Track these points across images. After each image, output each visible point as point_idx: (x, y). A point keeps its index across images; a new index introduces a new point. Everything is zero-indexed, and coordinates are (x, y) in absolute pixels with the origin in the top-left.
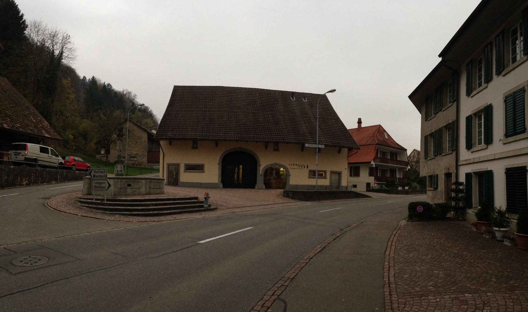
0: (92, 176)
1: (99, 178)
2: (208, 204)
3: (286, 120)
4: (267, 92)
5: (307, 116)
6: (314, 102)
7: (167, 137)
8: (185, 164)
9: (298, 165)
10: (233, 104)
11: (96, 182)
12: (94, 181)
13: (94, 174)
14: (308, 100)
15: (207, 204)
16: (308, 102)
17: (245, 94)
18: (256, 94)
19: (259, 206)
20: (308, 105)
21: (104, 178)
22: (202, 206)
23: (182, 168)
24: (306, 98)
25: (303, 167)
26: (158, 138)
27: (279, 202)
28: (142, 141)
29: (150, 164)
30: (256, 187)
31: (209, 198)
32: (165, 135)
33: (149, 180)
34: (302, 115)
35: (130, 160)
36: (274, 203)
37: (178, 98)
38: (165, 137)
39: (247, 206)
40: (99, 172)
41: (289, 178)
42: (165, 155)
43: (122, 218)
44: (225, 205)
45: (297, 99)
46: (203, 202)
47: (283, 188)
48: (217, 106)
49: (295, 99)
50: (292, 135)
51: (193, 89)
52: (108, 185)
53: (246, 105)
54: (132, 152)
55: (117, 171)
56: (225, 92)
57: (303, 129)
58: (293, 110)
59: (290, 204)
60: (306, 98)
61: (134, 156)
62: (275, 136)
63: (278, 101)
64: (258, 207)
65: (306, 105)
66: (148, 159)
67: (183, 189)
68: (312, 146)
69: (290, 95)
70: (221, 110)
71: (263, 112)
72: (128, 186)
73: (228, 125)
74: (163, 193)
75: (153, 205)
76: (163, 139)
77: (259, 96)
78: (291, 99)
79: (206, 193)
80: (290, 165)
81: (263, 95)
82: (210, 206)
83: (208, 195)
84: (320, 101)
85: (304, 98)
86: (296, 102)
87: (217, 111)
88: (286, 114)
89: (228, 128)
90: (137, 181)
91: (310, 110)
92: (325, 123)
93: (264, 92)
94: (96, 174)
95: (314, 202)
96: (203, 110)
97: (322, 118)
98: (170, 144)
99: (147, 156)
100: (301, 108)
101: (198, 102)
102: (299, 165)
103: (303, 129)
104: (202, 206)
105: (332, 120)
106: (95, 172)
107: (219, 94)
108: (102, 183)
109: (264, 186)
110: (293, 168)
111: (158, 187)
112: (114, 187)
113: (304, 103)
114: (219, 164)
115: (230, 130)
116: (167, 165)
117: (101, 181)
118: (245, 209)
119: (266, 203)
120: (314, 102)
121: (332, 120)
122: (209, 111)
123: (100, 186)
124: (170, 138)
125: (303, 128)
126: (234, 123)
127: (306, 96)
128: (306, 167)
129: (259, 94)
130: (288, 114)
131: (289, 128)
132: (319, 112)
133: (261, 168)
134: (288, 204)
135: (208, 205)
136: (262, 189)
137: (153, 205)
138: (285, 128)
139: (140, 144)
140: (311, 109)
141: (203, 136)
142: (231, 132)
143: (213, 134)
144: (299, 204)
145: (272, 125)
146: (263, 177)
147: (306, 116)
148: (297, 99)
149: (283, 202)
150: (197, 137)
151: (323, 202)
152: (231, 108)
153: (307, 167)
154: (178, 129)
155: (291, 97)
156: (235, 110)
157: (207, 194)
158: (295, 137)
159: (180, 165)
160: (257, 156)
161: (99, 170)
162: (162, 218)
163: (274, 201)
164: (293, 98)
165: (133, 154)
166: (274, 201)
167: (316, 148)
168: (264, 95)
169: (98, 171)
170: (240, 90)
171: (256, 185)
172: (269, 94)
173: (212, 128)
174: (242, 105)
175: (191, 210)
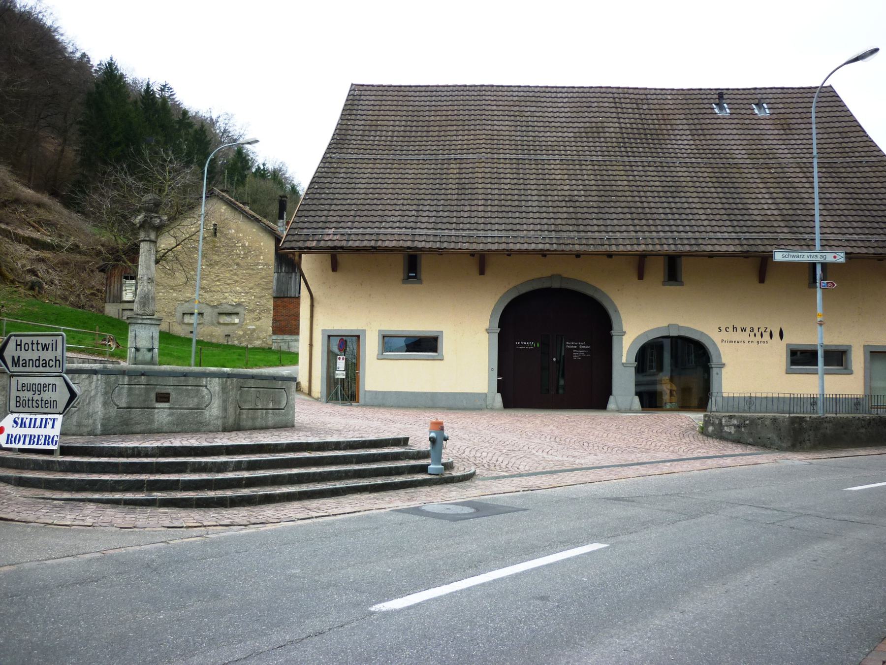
0: (9, 363)
1: (35, 369)
2: (443, 461)
3: (702, 179)
4: (638, 96)
5: (773, 161)
6: (791, 116)
7: (322, 244)
8: (379, 331)
9: (748, 330)
10: (531, 138)
11: (23, 385)
12: (14, 380)
13: (16, 355)
14: (772, 111)
15: (438, 460)
16: (775, 116)
17: (568, 105)
18: (601, 104)
19: (622, 466)
20: (772, 127)
21: (53, 369)
22: (424, 469)
23: (371, 346)
24: (765, 105)
25: (766, 336)
26: (292, 248)
27: (689, 456)
28: (258, 264)
29: (280, 337)
30: (611, 405)
31: (446, 439)
32: (317, 238)
33: (235, 380)
34: (755, 161)
35: (219, 323)
36: (673, 457)
37: (363, 122)
38: (314, 244)
39: (580, 466)
40: (35, 346)
41: (719, 374)
42: (315, 304)
43: (112, 515)
44: (503, 465)
45: (734, 111)
46: (424, 455)
47: (702, 404)
48: (483, 145)
49: (728, 111)
50: (725, 229)
51: (410, 94)
52: (68, 395)
53: (573, 139)
54: (226, 298)
55: (137, 349)
56: (506, 103)
57: (760, 207)
58: (724, 147)
59: (728, 461)
60: (765, 105)
61: (230, 309)
62: (670, 234)
63: (673, 122)
64: (620, 469)
65: (768, 127)
66: (275, 320)
67: (369, 412)
68: (799, 256)
69: (712, 101)
70: (496, 156)
71: (626, 159)
72: (157, 401)
73: (516, 203)
74: (289, 425)
75: (238, 466)
76: (310, 248)
77: (614, 110)
78: (717, 111)
79: (433, 424)
80: (723, 329)
81: (624, 105)
82: (448, 466)
83: (442, 429)
84: (819, 100)
85: (756, 104)
86: (732, 121)
87: (483, 160)
88: (699, 160)
89: (517, 215)
90: (190, 383)
91: (781, 142)
92: (838, 180)
93: (627, 96)
94: (25, 355)
95: (817, 455)
96: (440, 157)
97: (827, 165)
98: (335, 267)
99: (272, 312)
100: (749, 137)
101: (425, 134)
102: (752, 330)
103: (760, 207)
104: (424, 469)
105: (862, 169)
106: (20, 345)
107: (489, 108)
108: (45, 386)
109: (637, 400)
110: (731, 342)
111: (271, 406)
112: (105, 404)
113: (760, 122)
114: (488, 331)
115: (525, 221)
116: (323, 334)
117: (37, 380)
118: (574, 479)
119: (645, 458)
120: (791, 116)
121: (862, 169)
122: (458, 161)
123: (36, 397)
124: (335, 248)
125: (763, 201)
126: (536, 198)
127: (764, 96)
128: (776, 334)
129: (613, 105)
130: (706, 160)
131: (714, 206)
132: (820, 146)
133: (624, 342)
134: (721, 461)
135: (443, 464)
136: (631, 411)
137: (238, 466)
138: (698, 206)
139: (251, 272)
140: (785, 137)
141: (438, 239)
142: (525, 227)
143: (471, 233)
144: (759, 461)
145: (657, 199)
146: (632, 371)
147: (768, 161)
148: (734, 111)
149: (706, 455)
150: (416, 244)
151: (850, 453)
152: (526, 152)
153: (781, 335)
154: (357, 219)
155: (714, 106)
156: (539, 157)
157: (439, 427)
158: (734, 235)
159: (365, 336)
160: (616, 311)
161: (35, 339)
162: (268, 512)
163: (673, 452)
164: (721, 108)
165: (227, 303)
166: (673, 452)
167: (813, 265)
168: (629, 106)
169: (32, 344)
170: (554, 95)
171: (611, 398)
172: (645, 101)
173: (466, 215)
174: (561, 139)
175: (379, 481)
